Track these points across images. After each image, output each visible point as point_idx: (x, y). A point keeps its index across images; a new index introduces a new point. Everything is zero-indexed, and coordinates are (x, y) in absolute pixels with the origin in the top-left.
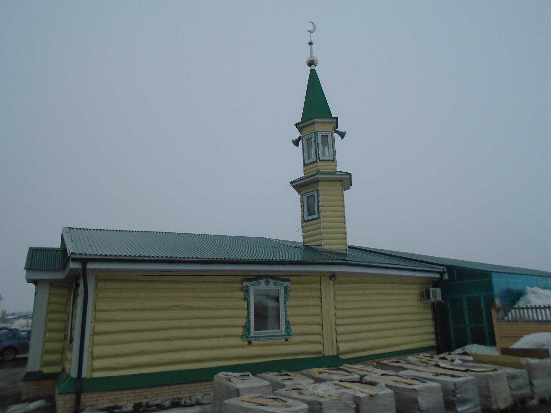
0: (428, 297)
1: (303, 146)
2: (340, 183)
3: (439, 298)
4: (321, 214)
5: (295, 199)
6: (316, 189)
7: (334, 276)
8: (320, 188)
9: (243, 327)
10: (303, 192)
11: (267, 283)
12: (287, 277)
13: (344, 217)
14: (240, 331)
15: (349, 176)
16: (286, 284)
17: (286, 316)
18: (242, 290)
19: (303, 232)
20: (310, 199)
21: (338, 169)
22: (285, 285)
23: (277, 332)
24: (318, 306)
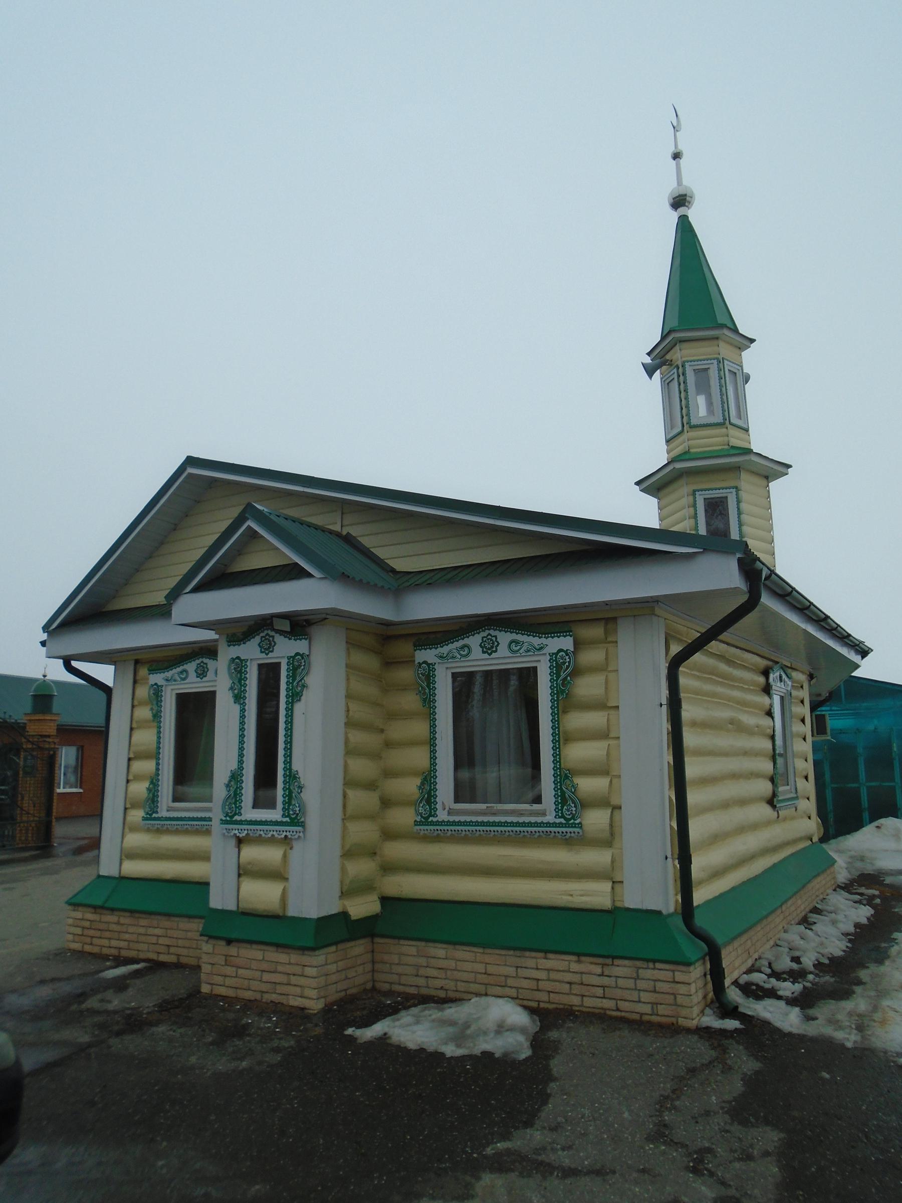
6: (732, 484)
11: (489, 648)
14: (765, 787)
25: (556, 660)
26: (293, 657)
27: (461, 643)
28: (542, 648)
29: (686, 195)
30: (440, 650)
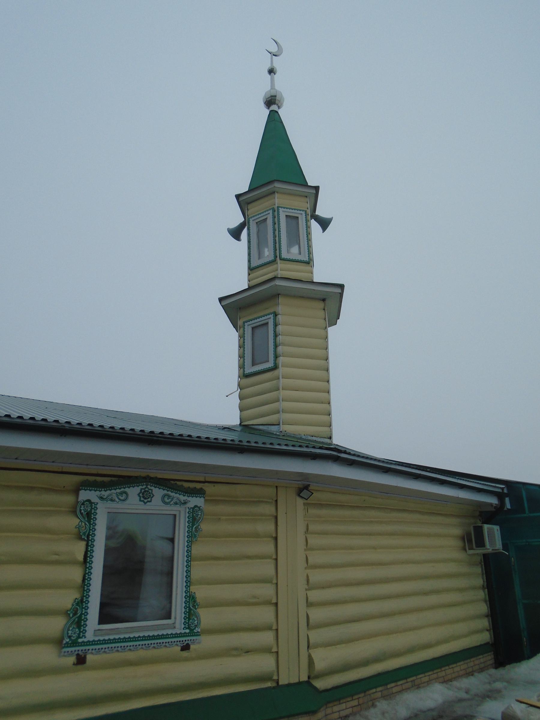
0: (481, 543)
1: (249, 242)
2: (321, 304)
3: (499, 545)
4: (281, 360)
5: (225, 339)
6: (272, 310)
7: (306, 487)
8: (280, 309)
9: (66, 613)
10: (245, 320)
11: (146, 497)
12: (198, 486)
13: (327, 370)
14: (56, 625)
15: (339, 291)
16: (195, 501)
17: (189, 582)
18: (74, 511)
19: (241, 398)
20: (258, 331)
21: (317, 279)
22: (191, 505)
23: (163, 627)
24: (270, 557)
26: (193, 508)
29: (276, 96)
30: (103, 493)
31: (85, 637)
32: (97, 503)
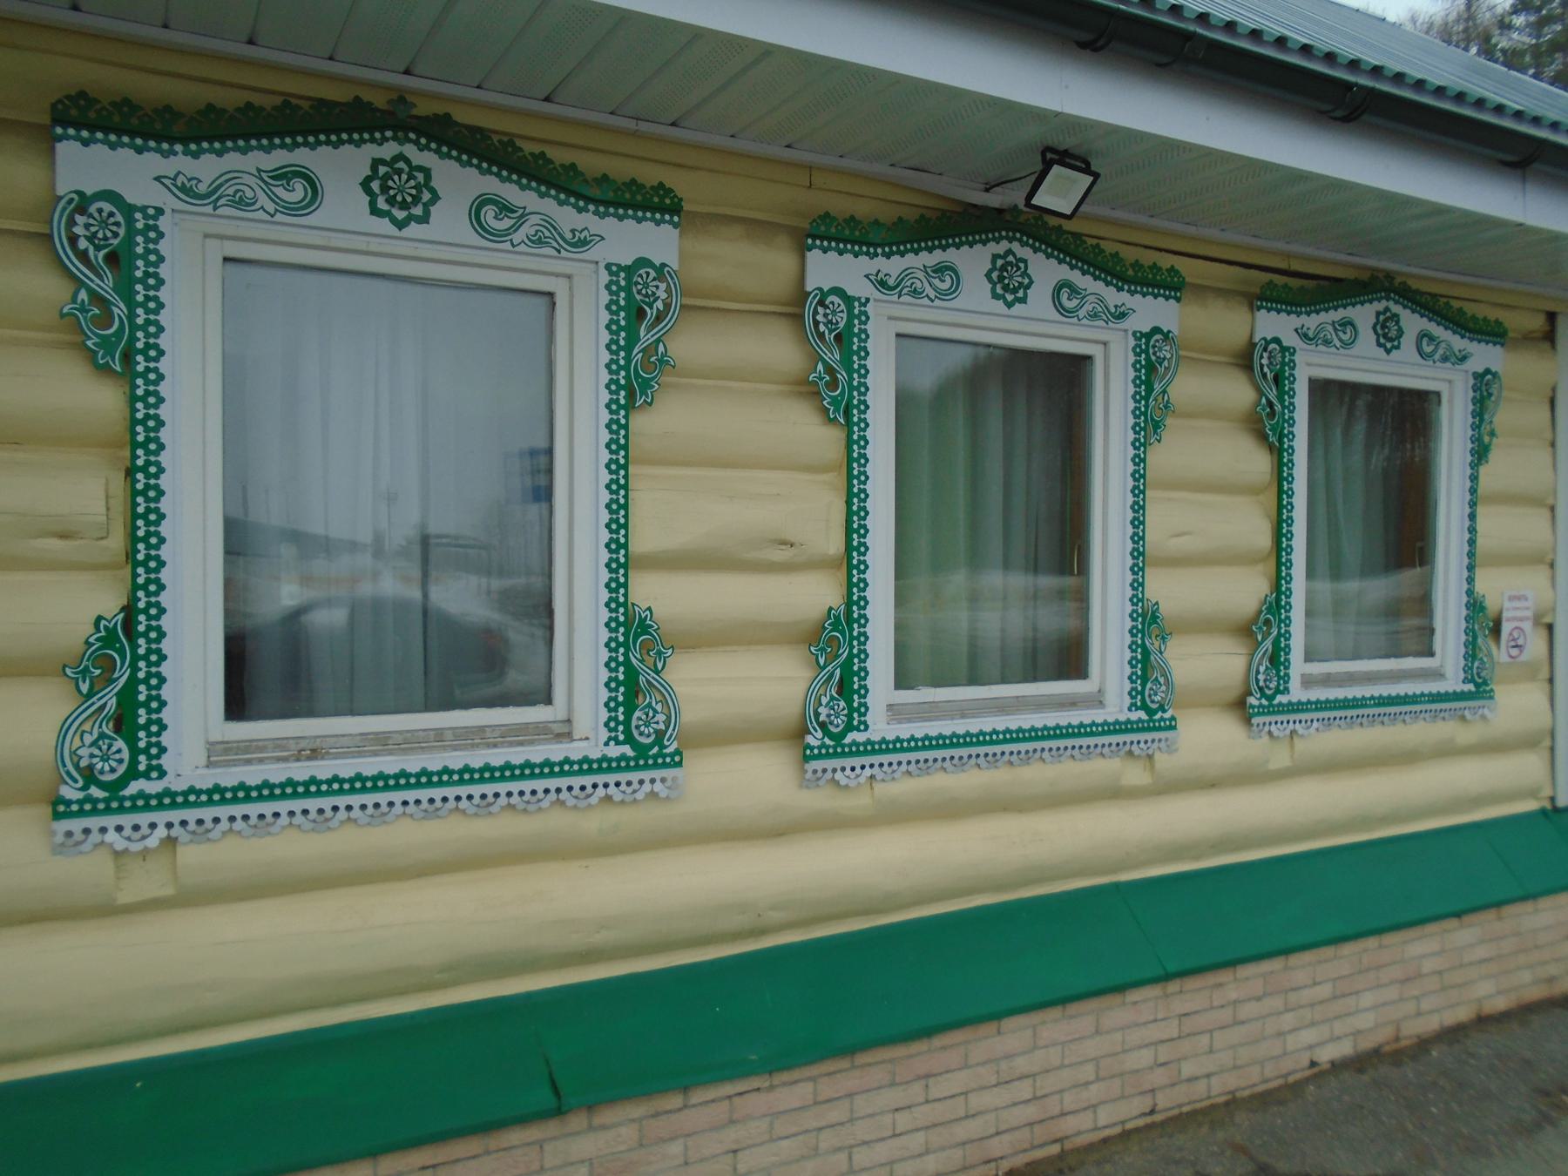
17: (621, 562)
22: (1476, 364)
25: (628, 289)
27: (937, 257)
28: (583, 243)
30: (880, 263)
31: (162, 774)
32: (868, 300)
